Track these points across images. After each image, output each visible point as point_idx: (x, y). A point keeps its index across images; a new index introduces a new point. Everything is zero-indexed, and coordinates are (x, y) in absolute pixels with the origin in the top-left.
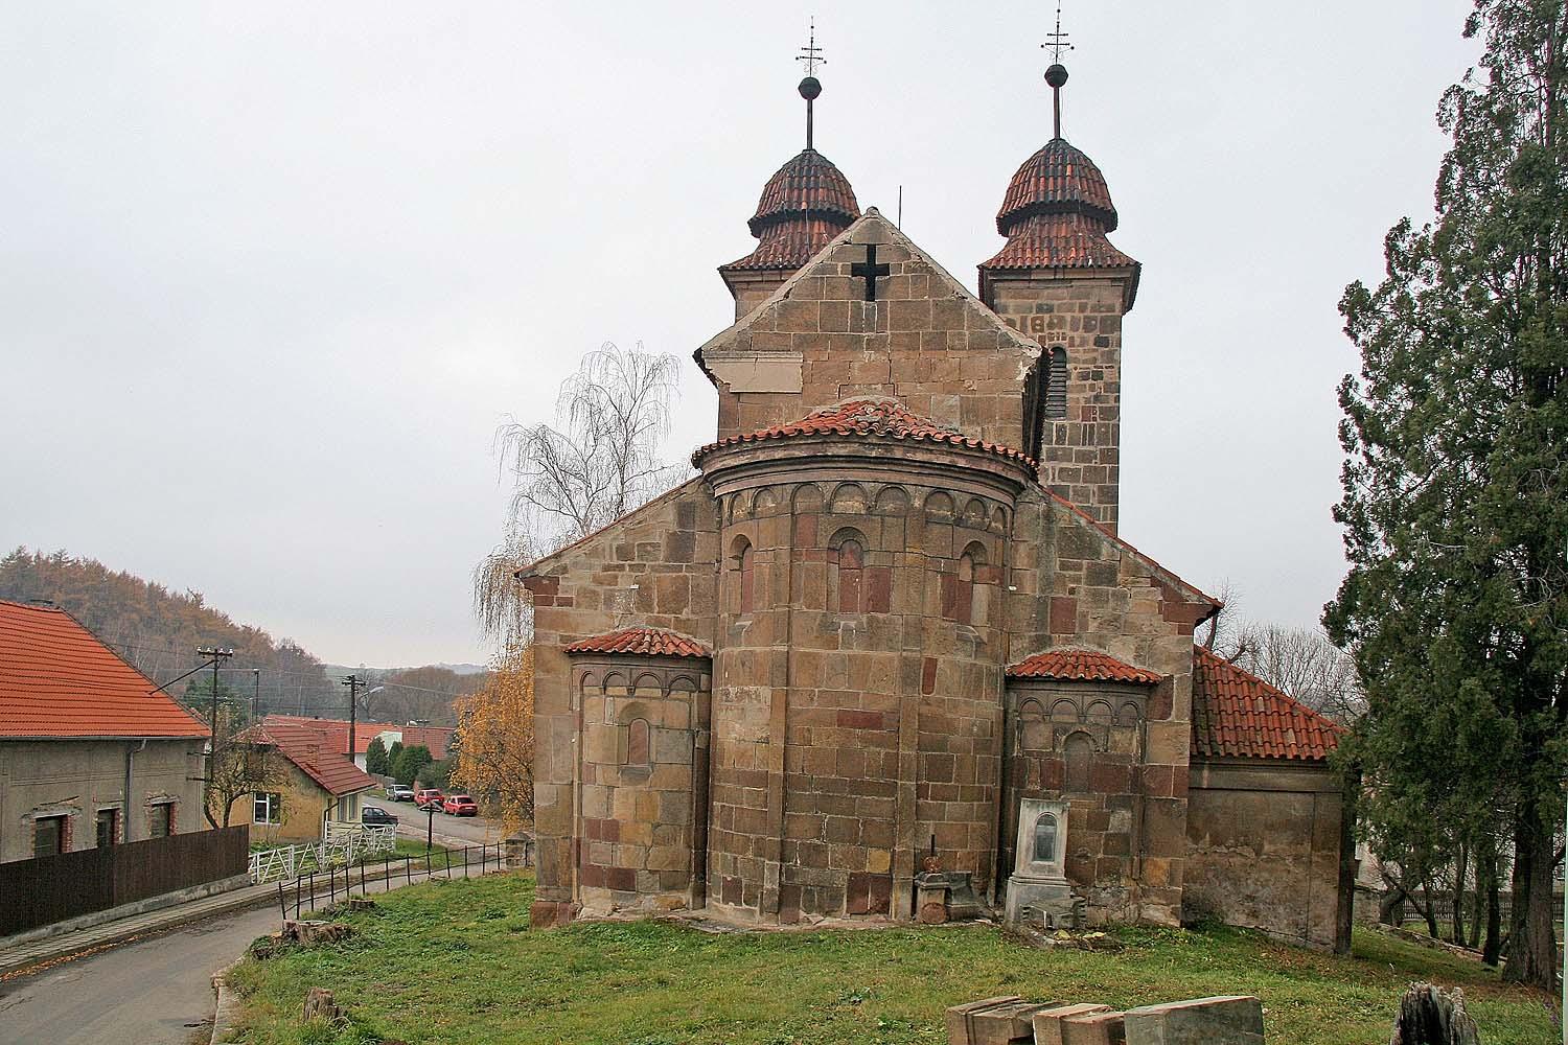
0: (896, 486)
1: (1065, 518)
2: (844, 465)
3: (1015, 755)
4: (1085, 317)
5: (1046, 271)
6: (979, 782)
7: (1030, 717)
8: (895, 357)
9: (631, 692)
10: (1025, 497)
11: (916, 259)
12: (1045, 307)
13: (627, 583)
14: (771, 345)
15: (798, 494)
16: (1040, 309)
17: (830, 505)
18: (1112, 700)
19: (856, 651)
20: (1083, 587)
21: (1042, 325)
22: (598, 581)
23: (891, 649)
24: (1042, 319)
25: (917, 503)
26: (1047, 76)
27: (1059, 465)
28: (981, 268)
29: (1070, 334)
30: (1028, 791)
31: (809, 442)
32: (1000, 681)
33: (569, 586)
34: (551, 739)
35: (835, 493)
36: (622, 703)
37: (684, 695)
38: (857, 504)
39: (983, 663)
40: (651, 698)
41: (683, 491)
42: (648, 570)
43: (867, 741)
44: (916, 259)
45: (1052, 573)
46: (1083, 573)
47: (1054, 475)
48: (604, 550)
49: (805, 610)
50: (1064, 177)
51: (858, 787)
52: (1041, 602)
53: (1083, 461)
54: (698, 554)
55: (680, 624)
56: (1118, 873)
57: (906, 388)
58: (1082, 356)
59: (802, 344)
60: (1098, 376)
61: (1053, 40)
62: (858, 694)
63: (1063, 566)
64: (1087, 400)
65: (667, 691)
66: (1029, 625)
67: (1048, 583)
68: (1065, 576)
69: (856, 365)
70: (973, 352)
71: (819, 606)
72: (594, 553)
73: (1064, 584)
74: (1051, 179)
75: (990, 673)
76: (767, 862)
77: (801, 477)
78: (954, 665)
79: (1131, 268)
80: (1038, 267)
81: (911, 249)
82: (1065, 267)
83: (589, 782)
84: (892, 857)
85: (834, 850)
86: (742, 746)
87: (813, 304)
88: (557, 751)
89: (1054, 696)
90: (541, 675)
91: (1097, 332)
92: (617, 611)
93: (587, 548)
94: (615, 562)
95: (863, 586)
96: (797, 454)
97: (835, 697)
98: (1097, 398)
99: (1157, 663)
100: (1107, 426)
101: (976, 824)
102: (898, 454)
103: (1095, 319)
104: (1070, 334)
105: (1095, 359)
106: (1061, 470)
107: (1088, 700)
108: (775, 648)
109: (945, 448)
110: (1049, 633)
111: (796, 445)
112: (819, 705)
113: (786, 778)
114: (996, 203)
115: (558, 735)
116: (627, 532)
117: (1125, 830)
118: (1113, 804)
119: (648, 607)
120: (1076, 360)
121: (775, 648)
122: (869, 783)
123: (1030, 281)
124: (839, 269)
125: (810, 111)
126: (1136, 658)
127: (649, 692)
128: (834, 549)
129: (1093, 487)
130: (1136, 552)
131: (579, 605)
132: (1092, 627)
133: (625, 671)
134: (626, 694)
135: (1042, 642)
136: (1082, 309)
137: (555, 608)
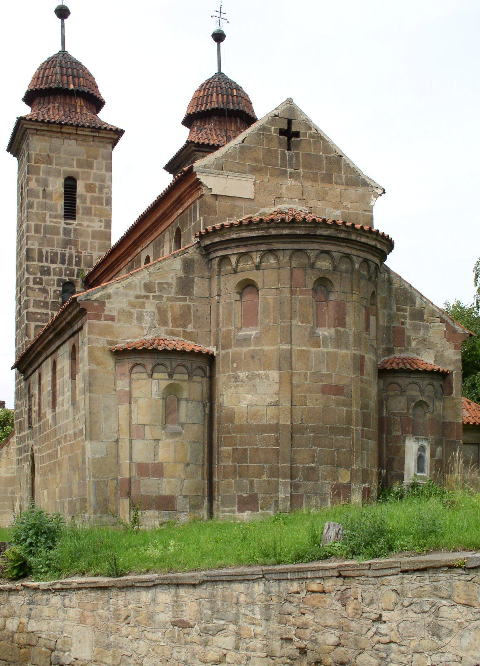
7: (392, 393)
8: (306, 184)
9: (170, 376)
11: (315, 131)
13: (151, 306)
14: (235, 169)
17: (313, 264)
19: (330, 349)
23: (347, 348)
25: (357, 266)
26: (225, 36)
36: (165, 383)
40: (185, 381)
41: (186, 251)
42: (165, 300)
43: (338, 403)
44: (315, 131)
45: (392, 312)
46: (407, 314)
49: (300, 324)
51: (334, 431)
54: (196, 291)
55: (187, 335)
57: (311, 203)
59: (254, 170)
62: (332, 375)
63: (399, 309)
65: (190, 376)
70: (347, 187)
71: (309, 322)
74: (220, 95)
76: (280, 480)
77: (297, 246)
81: (311, 125)
83: (139, 438)
85: (323, 470)
86: (254, 409)
87: (259, 148)
88: (107, 419)
89: (408, 380)
90: (94, 367)
92: (146, 325)
94: (143, 293)
96: (298, 232)
107: (426, 382)
108: (281, 347)
109: (374, 236)
110: (392, 346)
111: (298, 227)
113: (292, 425)
115: (106, 407)
119: (165, 323)
121: (281, 347)
122: (339, 427)
124: (273, 130)
125: (63, 26)
127: (180, 377)
130: (432, 304)
131: (119, 320)
132: (413, 344)
133: (167, 363)
134: (167, 377)
137: (103, 322)
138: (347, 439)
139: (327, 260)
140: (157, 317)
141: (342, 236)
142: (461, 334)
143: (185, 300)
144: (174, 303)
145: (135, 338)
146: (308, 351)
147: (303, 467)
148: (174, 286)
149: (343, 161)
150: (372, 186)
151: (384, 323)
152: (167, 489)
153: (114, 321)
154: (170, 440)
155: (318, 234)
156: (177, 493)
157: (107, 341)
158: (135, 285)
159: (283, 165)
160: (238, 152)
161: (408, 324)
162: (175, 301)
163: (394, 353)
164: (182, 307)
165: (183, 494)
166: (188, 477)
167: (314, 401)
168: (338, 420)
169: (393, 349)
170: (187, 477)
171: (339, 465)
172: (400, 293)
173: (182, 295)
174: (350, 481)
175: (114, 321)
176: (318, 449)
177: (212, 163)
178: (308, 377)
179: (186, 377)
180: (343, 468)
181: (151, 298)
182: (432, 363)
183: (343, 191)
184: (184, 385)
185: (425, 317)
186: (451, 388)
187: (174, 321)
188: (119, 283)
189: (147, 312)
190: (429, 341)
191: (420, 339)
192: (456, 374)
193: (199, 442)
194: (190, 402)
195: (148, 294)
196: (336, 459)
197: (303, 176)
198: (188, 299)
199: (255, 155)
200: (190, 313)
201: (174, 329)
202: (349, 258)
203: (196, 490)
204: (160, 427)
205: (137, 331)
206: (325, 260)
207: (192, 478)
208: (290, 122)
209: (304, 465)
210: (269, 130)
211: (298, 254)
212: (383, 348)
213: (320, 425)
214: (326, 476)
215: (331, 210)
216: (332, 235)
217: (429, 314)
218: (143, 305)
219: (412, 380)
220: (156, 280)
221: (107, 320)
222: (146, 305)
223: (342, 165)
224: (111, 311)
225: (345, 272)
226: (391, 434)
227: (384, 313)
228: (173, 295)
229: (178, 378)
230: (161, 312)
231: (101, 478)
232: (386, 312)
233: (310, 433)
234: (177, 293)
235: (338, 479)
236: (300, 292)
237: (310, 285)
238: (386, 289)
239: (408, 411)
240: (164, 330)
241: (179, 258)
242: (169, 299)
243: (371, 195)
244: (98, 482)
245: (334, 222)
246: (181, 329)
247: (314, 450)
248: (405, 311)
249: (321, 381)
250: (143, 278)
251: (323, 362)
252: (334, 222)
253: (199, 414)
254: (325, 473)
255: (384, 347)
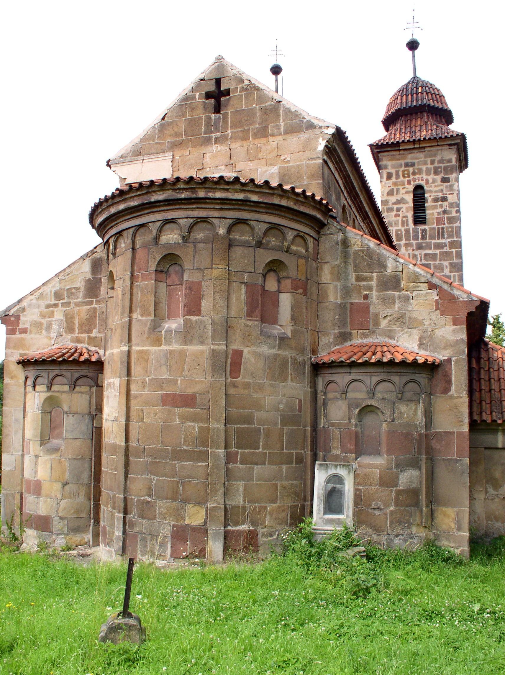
0: (205, 220)
1: (358, 243)
2: (165, 208)
3: (322, 426)
4: (434, 167)
5: (408, 143)
6: (287, 449)
8: (234, 146)
10: (327, 231)
11: (248, 83)
12: (410, 164)
13: (59, 315)
14: (153, 151)
15: (137, 234)
16: (407, 165)
18: (396, 379)
19: (176, 346)
20: (375, 293)
21: (408, 174)
22: (43, 316)
23: (202, 343)
24: (408, 171)
25: (222, 231)
27: (423, 252)
28: (371, 146)
29: (425, 177)
30: (333, 456)
31: (138, 193)
32: (308, 369)
33: (26, 320)
34: (13, 424)
35: (160, 230)
36: (44, 396)
37: (86, 389)
38: (175, 236)
39: (286, 353)
40: (64, 392)
41: (95, 250)
42: (72, 305)
43: (185, 418)
44: (248, 83)
45: (349, 284)
46: (374, 283)
47: (421, 258)
48: (47, 294)
49: (140, 318)
50: (417, 94)
52: (342, 307)
53: (438, 248)
55: (91, 341)
56: (408, 522)
58: (433, 189)
60: (444, 199)
61: (411, 26)
62: (177, 380)
63: (359, 279)
64: (439, 214)
65: (74, 385)
66: (333, 324)
67: (347, 292)
68: (360, 286)
69: (208, 155)
70: (287, 136)
71: (149, 315)
72: (41, 297)
73: (359, 292)
75: (295, 362)
78: (258, 355)
79: (460, 137)
80: (403, 142)
81: (244, 77)
82: (419, 140)
84: (207, 511)
87: (180, 121)
89: (348, 378)
91: (442, 175)
92: (53, 335)
93: (37, 294)
94: (53, 302)
95: (181, 296)
97: (160, 384)
98: (445, 212)
99: (436, 349)
100: (452, 228)
101: (285, 483)
102: (201, 194)
103: (440, 167)
104: (425, 177)
105: (442, 190)
106: (426, 255)
110: (349, 330)
111: (131, 197)
112: (148, 391)
114: (382, 114)
116: (60, 282)
117: (414, 486)
118: (401, 466)
120: (430, 192)
123: (399, 150)
124: (197, 97)
126: (421, 345)
128: (162, 272)
129: (446, 263)
132: (384, 323)
134: (46, 389)
135: (345, 337)
136: (432, 163)
137: (18, 336)
138: (200, 466)
139: (175, 232)
140: (65, 325)
141: (183, 196)
142: (464, 301)
143: (91, 303)
144: (81, 308)
145: (44, 349)
146: (148, 351)
147: (138, 500)
148: (82, 290)
149: (282, 106)
150: (320, 127)
151: (336, 299)
152: (43, 509)
153: (26, 333)
154: (47, 457)
155: (152, 200)
156: (53, 514)
157: (20, 354)
158: (47, 294)
159: (208, 131)
160: (157, 131)
161: (374, 297)
162: (82, 306)
163: (351, 340)
164: (88, 311)
165: (59, 515)
166: (65, 498)
167: (152, 415)
168: (185, 441)
169: (350, 334)
170: (63, 497)
171: (186, 501)
172: (363, 257)
173: (89, 298)
174: (205, 522)
175: (26, 333)
176: (156, 478)
177: (129, 151)
178: (146, 385)
179: (66, 388)
180: (192, 505)
181: (60, 305)
182: (415, 348)
183: (282, 142)
184: (64, 397)
185: (403, 284)
186: (449, 382)
187: (81, 327)
188: (32, 294)
189: (55, 320)
190: (410, 318)
191: (395, 316)
192: (457, 361)
193: (82, 459)
194: (71, 415)
195: (57, 302)
196: (180, 492)
197: (231, 138)
198: (94, 302)
199: (176, 130)
200: (96, 317)
201: (79, 335)
202: (248, 224)
203: (77, 511)
204: (39, 442)
205: (46, 341)
206: (173, 231)
207: (70, 498)
208: (218, 82)
209: (139, 498)
210: (194, 98)
211: (142, 230)
212: (335, 334)
213: (159, 447)
214: (166, 513)
215: (265, 168)
216: (171, 198)
217: (409, 279)
218: (52, 314)
219: (353, 377)
220: (65, 286)
221: (20, 333)
222: (55, 313)
223: (281, 111)
224: (24, 324)
225: (202, 242)
226: (329, 452)
227: (336, 287)
228: (80, 300)
229: (56, 389)
230: (69, 318)
231: (9, 490)
232: (339, 284)
233: (147, 456)
234: (85, 297)
235: (183, 519)
236: (142, 277)
237: (153, 266)
238: (340, 254)
239: (350, 420)
240: (70, 337)
241: (87, 259)
242: (77, 305)
243: (319, 138)
244: (7, 494)
245: (267, 183)
246: (85, 335)
247: (151, 479)
248: (371, 279)
249: (162, 389)
250: (54, 286)
251: (165, 364)
252: (267, 183)
253: (84, 428)
254: (164, 510)
255: (336, 331)
